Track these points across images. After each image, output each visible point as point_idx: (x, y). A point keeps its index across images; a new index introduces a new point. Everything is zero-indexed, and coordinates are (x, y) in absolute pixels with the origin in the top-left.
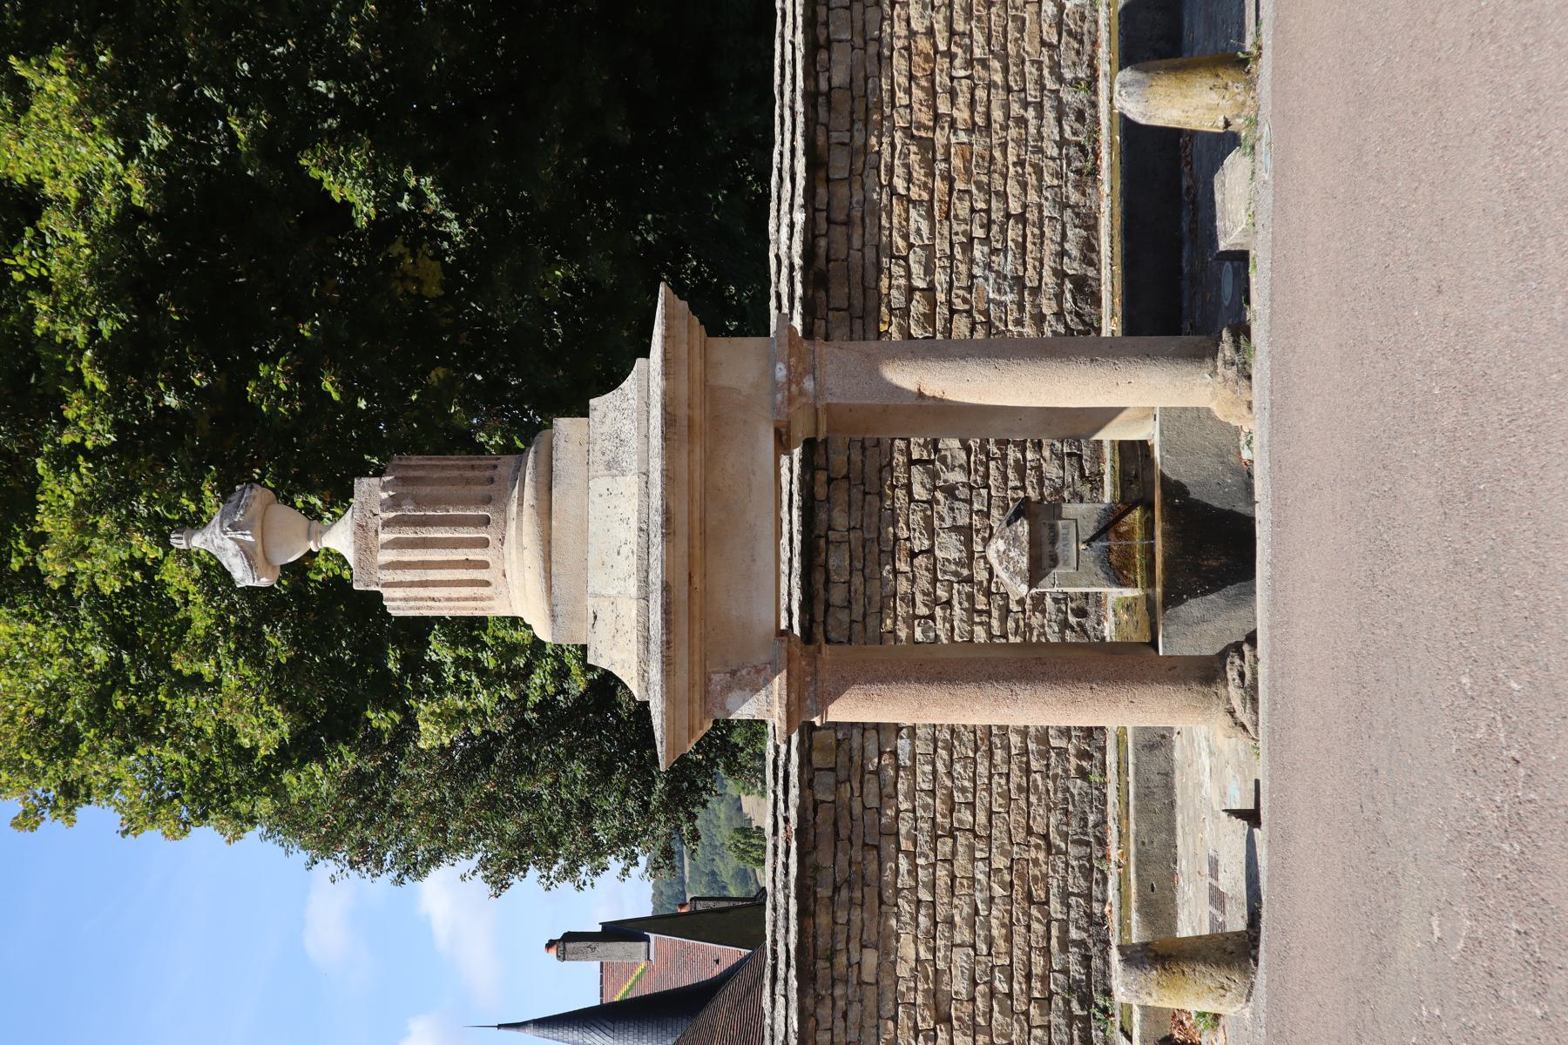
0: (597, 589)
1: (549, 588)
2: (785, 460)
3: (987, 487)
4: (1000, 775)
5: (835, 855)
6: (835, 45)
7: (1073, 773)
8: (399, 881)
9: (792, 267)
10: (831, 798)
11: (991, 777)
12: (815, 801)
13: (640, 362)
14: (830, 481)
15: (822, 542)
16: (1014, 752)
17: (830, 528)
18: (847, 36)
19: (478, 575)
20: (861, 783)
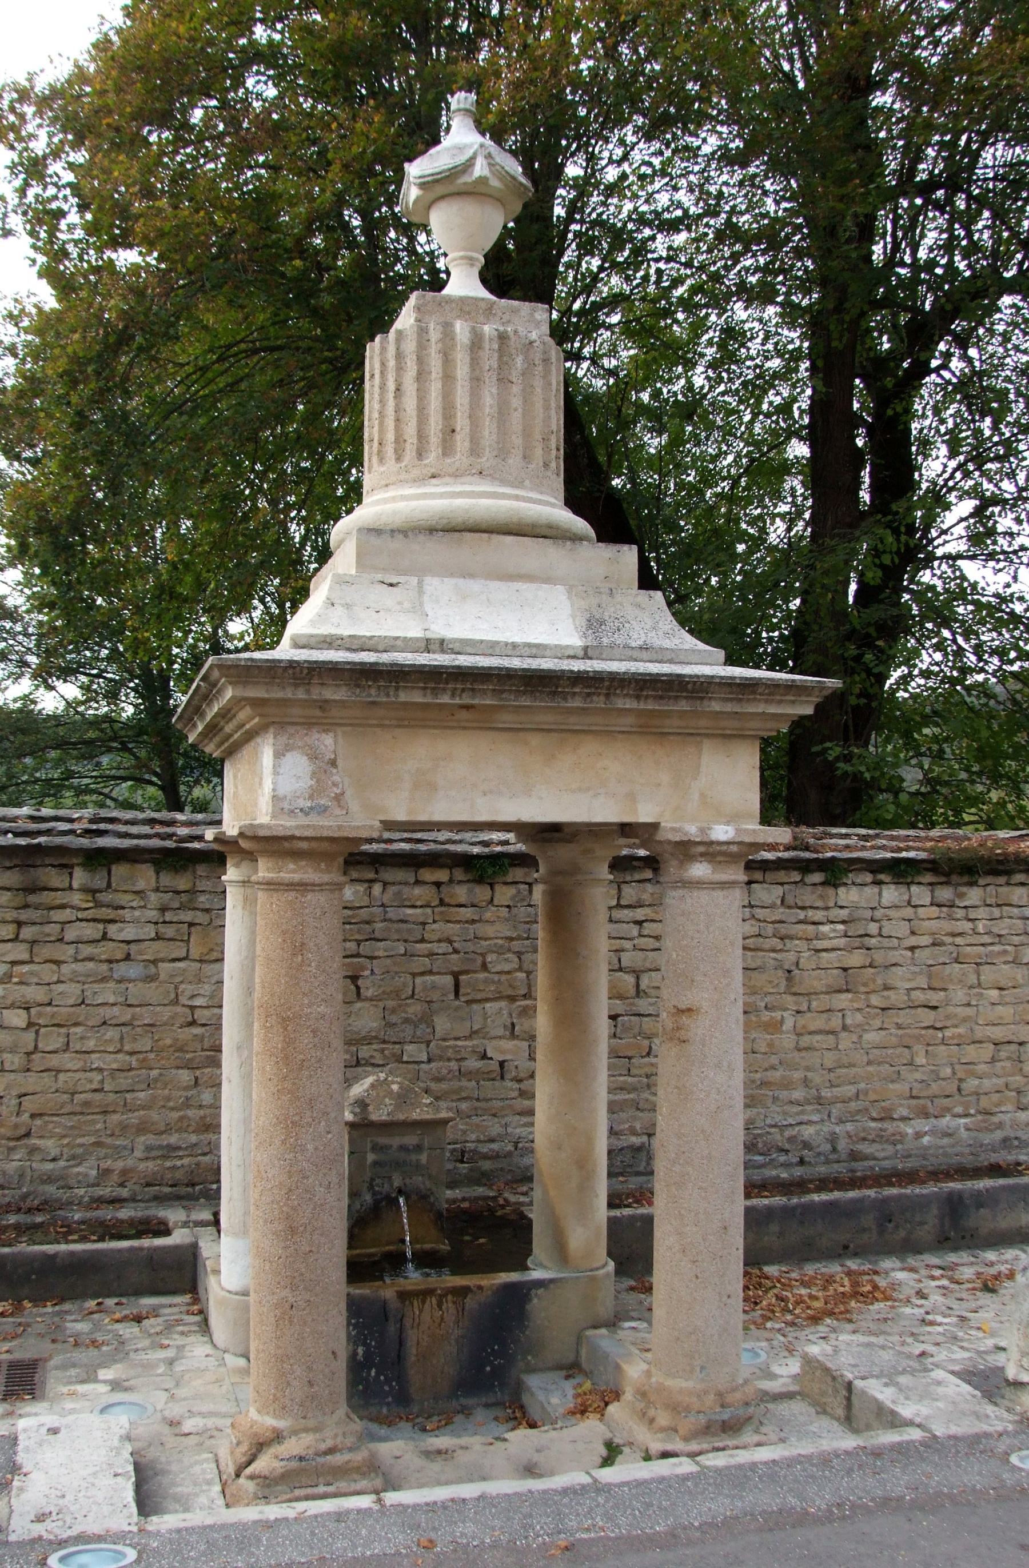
0: (428, 588)
1: (432, 530)
2: (511, 836)
3: (429, 1061)
4: (102, 1082)
5: (8, 889)
6: (876, 890)
7: (104, 1165)
8: (76, 61)
9: (900, 850)
10: (75, 885)
11: (100, 1070)
12: (72, 867)
13: (720, 654)
14: (438, 884)
15: (371, 875)
16: (128, 1096)
17: (385, 884)
18: (885, 902)
19: (439, 446)
20: (94, 920)
